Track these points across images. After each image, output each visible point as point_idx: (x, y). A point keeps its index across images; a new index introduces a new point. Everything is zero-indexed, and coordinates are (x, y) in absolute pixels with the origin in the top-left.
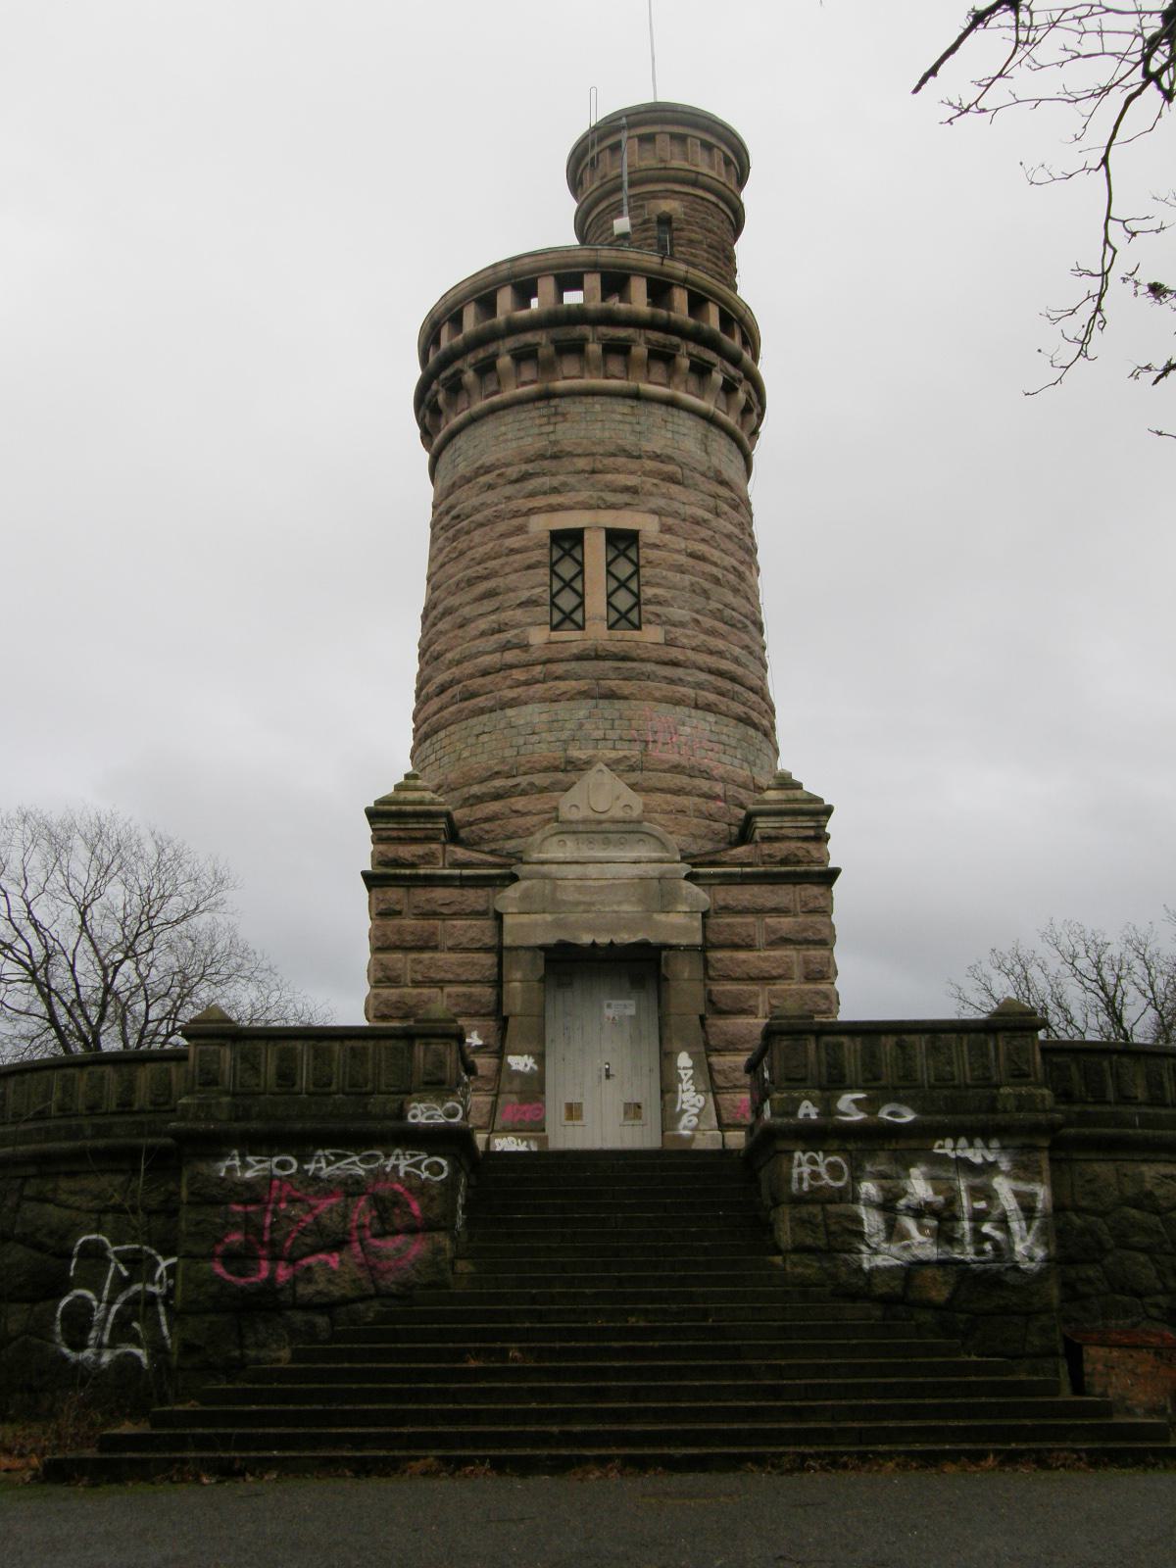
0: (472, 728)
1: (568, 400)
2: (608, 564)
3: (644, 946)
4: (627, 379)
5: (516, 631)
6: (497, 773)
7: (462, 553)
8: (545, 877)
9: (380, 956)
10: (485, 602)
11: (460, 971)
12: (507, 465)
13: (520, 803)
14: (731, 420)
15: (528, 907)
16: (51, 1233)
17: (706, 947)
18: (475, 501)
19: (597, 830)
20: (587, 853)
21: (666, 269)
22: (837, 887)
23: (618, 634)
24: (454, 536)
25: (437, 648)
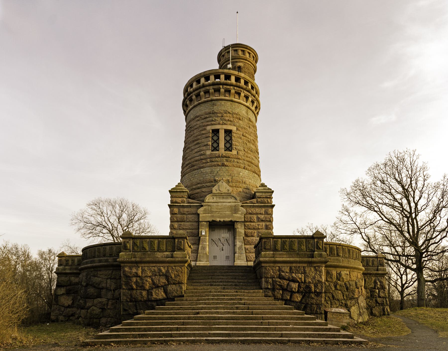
0: (193, 173)
1: (216, 101)
2: (225, 137)
3: (231, 221)
4: (230, 97)
5: (203, 151)
6: (199, 183)
7: (192, 135)
8: (209, 206)
9: (172, 223)
10: (197, 145)
11: (190, 227)
12: (202, 115)
13: (204, 190)
14: (253, 108)
15: (205, 212)
16: (97, 284)
17: (245, 221)
18: (195, 124)
19: (221, 195)
20: (219, 200)
21: (239, 75)
22: (274, 209)
23: (227, 152)
24: (190, 132)
25: (186, 156)
